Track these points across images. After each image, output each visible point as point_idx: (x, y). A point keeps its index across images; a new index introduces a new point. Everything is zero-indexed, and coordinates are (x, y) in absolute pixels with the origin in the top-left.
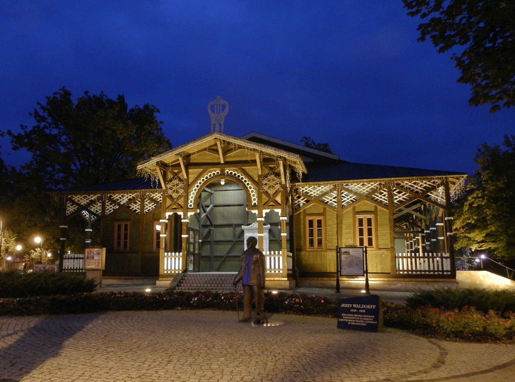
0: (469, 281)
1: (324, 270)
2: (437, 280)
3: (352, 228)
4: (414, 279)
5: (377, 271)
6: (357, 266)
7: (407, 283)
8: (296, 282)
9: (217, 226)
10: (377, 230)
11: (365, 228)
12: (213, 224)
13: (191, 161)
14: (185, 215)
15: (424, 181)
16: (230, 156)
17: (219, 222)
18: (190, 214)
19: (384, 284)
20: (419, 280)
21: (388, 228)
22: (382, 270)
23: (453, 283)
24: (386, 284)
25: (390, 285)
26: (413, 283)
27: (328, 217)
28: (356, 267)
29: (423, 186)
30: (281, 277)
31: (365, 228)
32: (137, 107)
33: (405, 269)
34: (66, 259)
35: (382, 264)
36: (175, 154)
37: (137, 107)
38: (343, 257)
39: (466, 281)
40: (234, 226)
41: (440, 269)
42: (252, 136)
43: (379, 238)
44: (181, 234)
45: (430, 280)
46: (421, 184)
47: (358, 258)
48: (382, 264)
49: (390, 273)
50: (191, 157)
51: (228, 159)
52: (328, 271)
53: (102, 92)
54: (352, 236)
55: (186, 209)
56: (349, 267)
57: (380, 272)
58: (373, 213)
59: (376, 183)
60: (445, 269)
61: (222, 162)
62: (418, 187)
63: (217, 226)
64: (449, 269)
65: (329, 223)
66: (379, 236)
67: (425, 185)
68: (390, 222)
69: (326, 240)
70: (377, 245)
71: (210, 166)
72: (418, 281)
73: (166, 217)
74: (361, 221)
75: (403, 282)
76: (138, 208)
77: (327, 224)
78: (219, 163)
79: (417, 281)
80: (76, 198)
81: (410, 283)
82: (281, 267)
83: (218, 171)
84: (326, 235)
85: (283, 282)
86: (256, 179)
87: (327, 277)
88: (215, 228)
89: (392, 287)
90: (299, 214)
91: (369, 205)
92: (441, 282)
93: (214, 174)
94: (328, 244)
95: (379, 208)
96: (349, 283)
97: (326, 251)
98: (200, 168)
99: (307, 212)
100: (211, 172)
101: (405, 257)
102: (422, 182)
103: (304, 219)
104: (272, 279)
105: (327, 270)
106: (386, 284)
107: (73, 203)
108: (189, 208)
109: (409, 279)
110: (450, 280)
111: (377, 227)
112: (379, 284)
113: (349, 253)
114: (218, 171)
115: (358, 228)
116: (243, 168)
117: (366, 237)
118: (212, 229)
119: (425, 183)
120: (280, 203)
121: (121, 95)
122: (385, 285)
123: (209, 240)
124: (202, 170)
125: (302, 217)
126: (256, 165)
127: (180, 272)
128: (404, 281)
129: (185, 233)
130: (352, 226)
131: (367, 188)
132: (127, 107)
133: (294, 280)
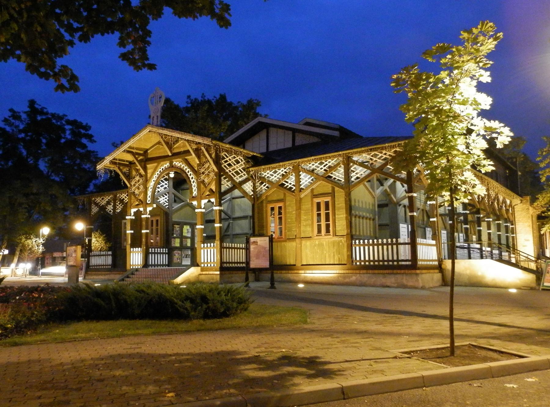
0: (468, 272)
1: (284, 263)
2: (395, 271)
3: (311, 213)
4: (371, 271)
5: (334, 262)
6: (264, 256)
7: (362, 275)
8: (256, 275)
9: (235, 219)
10: (334, 214)
11: (323, 212)
12: (232, 217)
13: (149, 156)
14: (145, 210)
15: (384, 152)
16: (176, 148)
17: (238, 214)
18: (149, 209)
19: (338, 277)
20: (376, 271)
21: (344, 211)
22: (339, 260)
23: (413, 275)
24: (341, 277)
25: (345, 278)
26: (368, 275)
27: (287, 203)
28: (263, 258)
29: (382, 158)
30: (214, 271)
31: (323, 212)
32: (240, 104)
33: (386, 258)
34: (92, 256)
35: (339, 254)
36: (123, 151)
37: (240, 104)
38: (252, 247)
39: (465, 273)
40: (249, 218)
41: (395, 258)
42: (257, 122)
43: (336, 224)
44: (141, 229)
45: (387, 271)
46: (380, 155)
47: (265, 248)
48: (339, 254)
49: (345, 264)
50: (149, 152)
51: (176, 151)
52: (288, 263)
53: (203, 94)
54: (310, 222)
55: (146, 205)
56: (256, 259)
57: (337, 263)
58: (329, 195)
59: (333, 160)
60: (401, 258)
61: (170, 154)
62: (377, 159)
63: (235, 219)
64: (409, 257)
65: (289, 209)
66: (336, 222)
67: (385, 156)
68: (346, 204)
69: (285, 229)
70: (334, 232)
71: (160, 160)
72: (375, 273)
73: (131, 214)
74: (319, 204)
75: (358, 275)
76: (118, 206)
77: (287, 210)
78: (168, 156)
79: (373, 274)
80: (98, 200)
81: (365, 275)
82: (215, 261)
83: (167, 164)
84: (285, 224)
85: (215, 275)
86: (196, 169)
87: (282, 269)
88: (233, 220)
89: (347, 280)
90: (262, 202)
91: (327, 187)
92: (400, 273)
93: (163, 169)
94: (288, 233)
95: (336, 189)
96: (305, 277)
97: (285, 241)
98: (154, 163)
99: (269, 199)
100: (162, 165)
101: (385, 244)
102: (381, 153)
103: (266, 206)
104: (207, 273)
105: (286, 263)
106: (341, 277)
107: (97, 204)
108: (148, 204)
109: (365, 271)
110: (410, 271)
111: (335, 210)
112: (331, 277)
113: (257, 242)
114: (167, 164)
115: (315, 213)
116: (186, 158)
117: (323, 223)
118: (231, 222)
119: (385, 154)
120: (214, 190)
121: (223, 94)
122: (340, 278)
123: (228, 233)
124: (156, 164)
125: (264, 204)
126: (192, 155)
127: (139, 267)
128: (359, 274)
129: (145, 228)
130: (310, 211)
131: (324, 166)
132: (163, 108)
133: (440, 273)
